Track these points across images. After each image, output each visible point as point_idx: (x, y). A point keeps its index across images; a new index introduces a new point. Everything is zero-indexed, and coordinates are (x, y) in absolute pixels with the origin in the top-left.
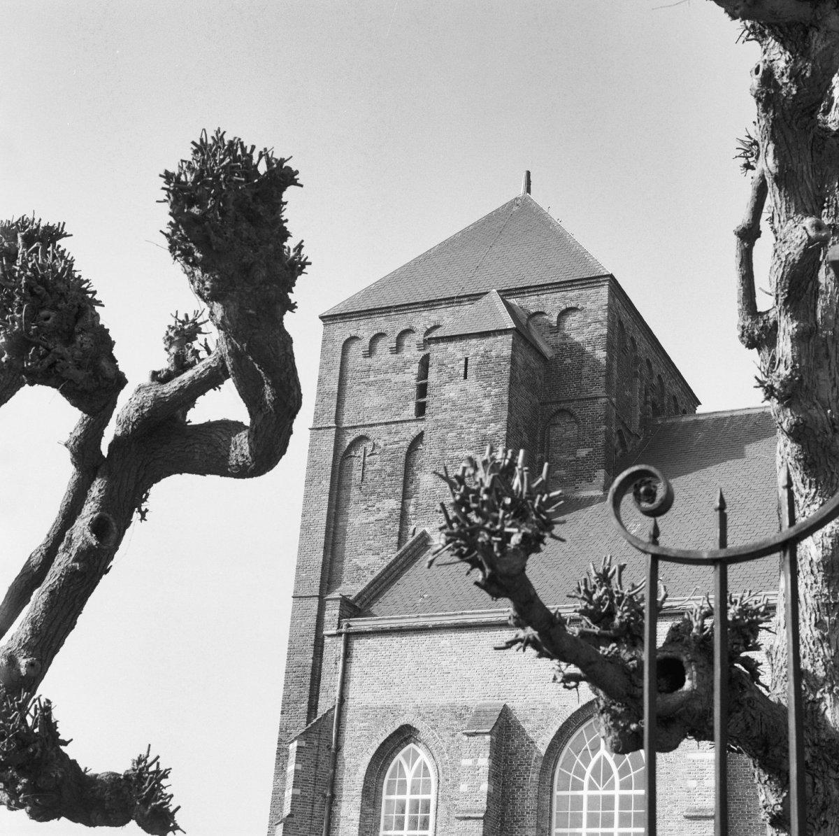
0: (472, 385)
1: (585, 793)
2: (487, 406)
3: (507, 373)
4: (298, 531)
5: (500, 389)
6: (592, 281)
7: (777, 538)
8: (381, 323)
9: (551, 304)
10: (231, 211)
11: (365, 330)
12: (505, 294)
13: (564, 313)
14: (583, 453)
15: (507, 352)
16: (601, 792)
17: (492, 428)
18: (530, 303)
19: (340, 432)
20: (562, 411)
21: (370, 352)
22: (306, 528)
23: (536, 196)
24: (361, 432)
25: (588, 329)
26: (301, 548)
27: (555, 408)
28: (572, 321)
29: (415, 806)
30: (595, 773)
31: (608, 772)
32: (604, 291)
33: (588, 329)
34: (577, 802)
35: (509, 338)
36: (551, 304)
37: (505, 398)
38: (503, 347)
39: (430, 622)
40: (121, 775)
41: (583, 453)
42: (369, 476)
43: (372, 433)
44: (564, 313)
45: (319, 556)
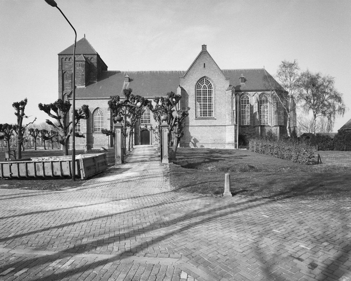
0: (80, 67)
1: (97, 117)
2: (82, 70)
3: (85, 67)
4: (58, 84)
5: (84, 68)
6: (95, 54)
7: (20, 202)
8: (67, 56)
9: (90, 57)
10: (164, 217)
11: (65, 57)
12: (83, 54)
13: (91, 58)
14: (94, 76)
15: (84, 64)
16: (99, 117)
17: (83, 73)
18: (87, 56)
19: (62, 71)
20: (91, 71)
21: (65, 60)
22: (59, 83)
23: (86, 38)
24: (65, 71)
25: (94, 61)
26: (59, 86)
27: (91, 71)
28: (92, 59)
29: (148, 113)
30: (98, 115)
31: (99, 115)
32: (96, 56)
33: (94, 61)
34: (96, 121)
35: (85, 62)
36: (90, 57)
37: (85, 70)
38: (84, 63)
39: (79, 99)
40: (332, 131)
41: (94, 76)
42: (67, 77)
43: (67, 71)
44: (91, 58)
45: (61, 87)
